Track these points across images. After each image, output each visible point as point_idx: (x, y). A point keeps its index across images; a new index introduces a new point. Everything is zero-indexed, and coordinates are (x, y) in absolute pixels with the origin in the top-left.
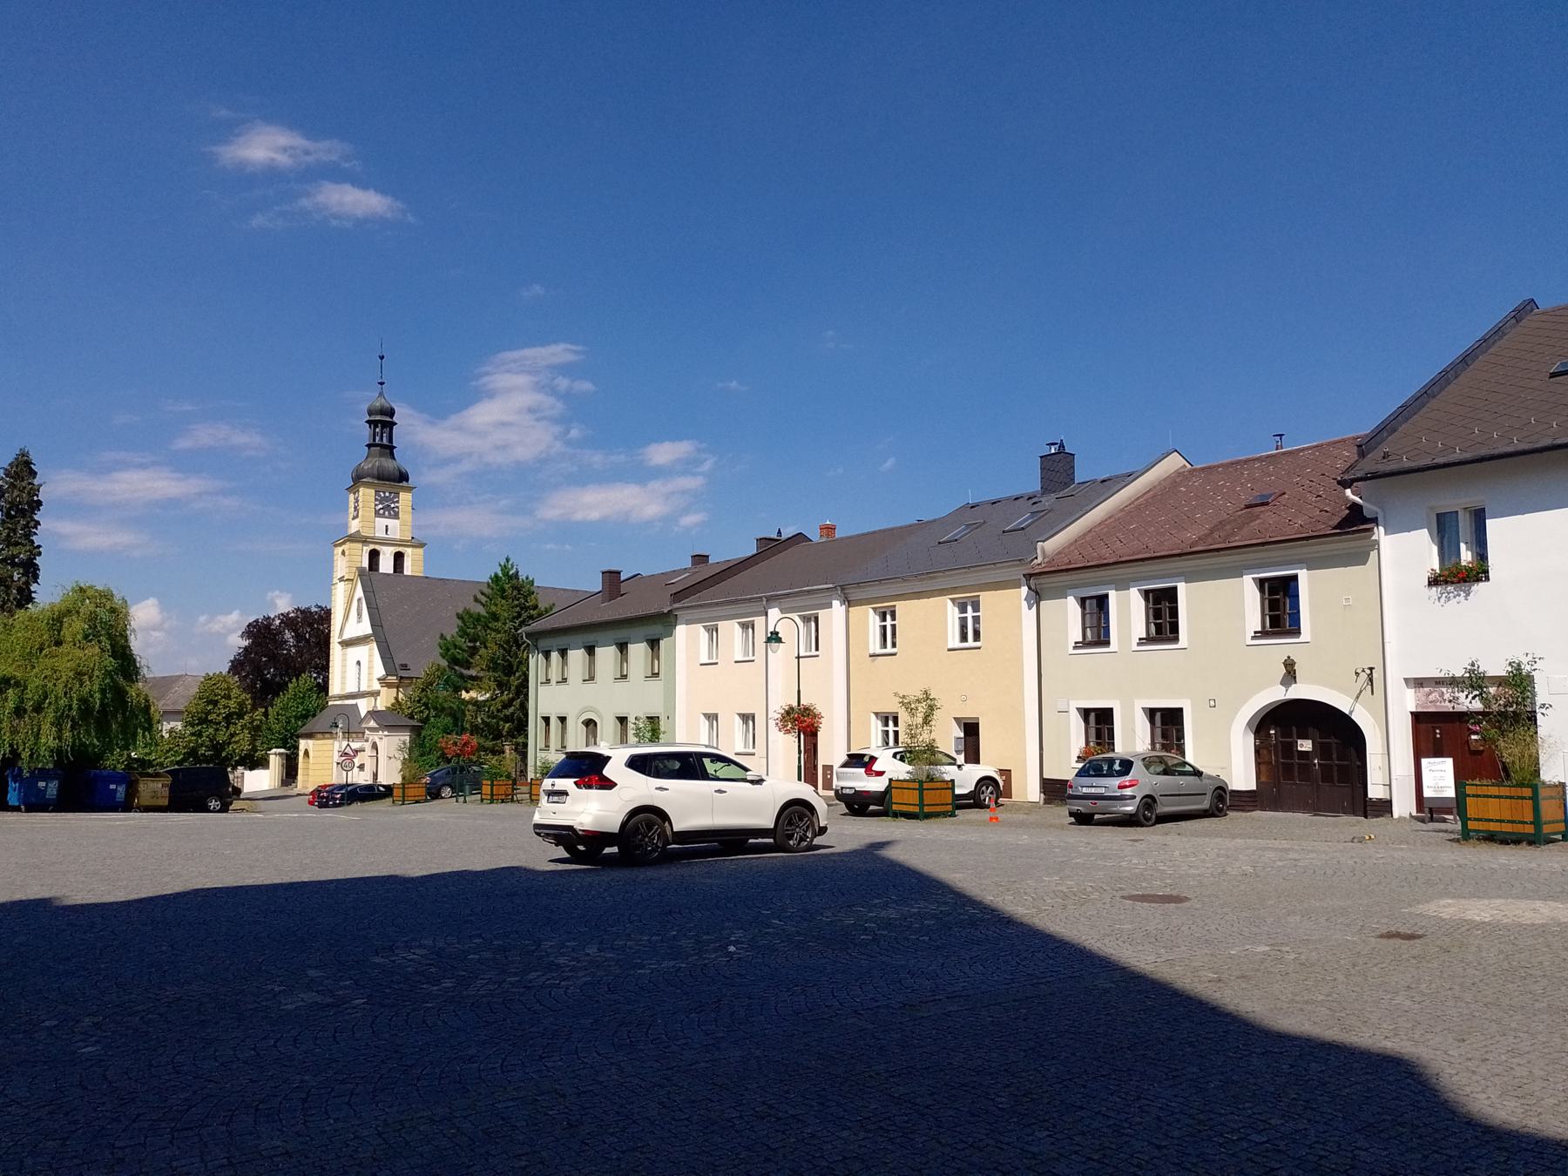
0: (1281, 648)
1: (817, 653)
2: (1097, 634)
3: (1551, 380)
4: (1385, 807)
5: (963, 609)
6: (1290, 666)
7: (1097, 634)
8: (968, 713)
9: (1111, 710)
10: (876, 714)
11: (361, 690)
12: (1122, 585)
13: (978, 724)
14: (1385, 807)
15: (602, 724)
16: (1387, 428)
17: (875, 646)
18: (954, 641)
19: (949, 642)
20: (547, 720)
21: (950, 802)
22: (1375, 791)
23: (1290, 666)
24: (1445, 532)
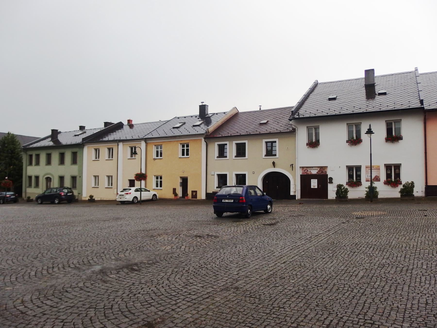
0: (271, 159)
1: (161, 158)
2: (222, 153)
3: (335, 97)
4: (294, 196)
5: (157, 148)
6: (274, 163)
7: (222, 153)
8: (184, 175)
9: (227, 174)
10: (155, 176)
11: (262, 109)
12: (231, 141)
13: (187, 179)
14: (294, 196)
15: (54, 179)
16: (301, 104)
17: (154, 156)
18: (180, 155)
19: (179, 155)
20: (30, 177)
21: (140, 192)
22: (292, 193)
23: (274, 163)
24: (157, 147)
